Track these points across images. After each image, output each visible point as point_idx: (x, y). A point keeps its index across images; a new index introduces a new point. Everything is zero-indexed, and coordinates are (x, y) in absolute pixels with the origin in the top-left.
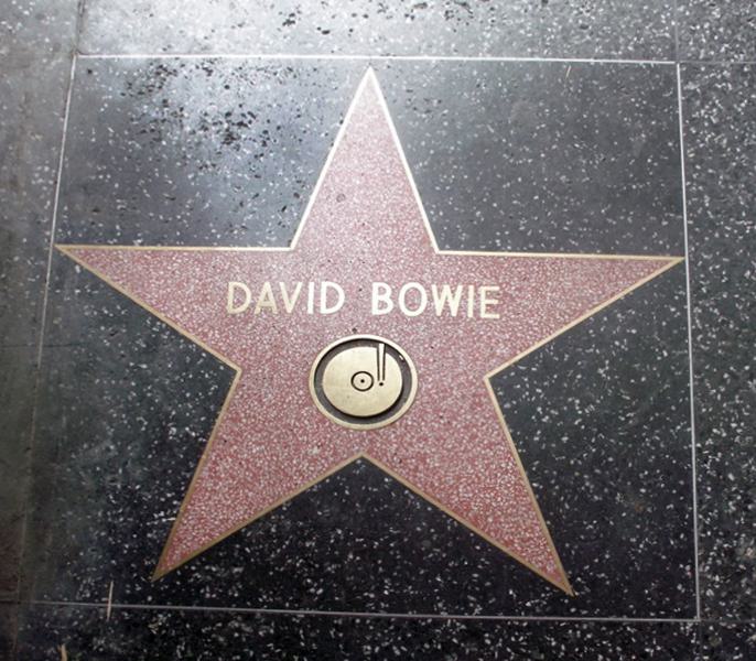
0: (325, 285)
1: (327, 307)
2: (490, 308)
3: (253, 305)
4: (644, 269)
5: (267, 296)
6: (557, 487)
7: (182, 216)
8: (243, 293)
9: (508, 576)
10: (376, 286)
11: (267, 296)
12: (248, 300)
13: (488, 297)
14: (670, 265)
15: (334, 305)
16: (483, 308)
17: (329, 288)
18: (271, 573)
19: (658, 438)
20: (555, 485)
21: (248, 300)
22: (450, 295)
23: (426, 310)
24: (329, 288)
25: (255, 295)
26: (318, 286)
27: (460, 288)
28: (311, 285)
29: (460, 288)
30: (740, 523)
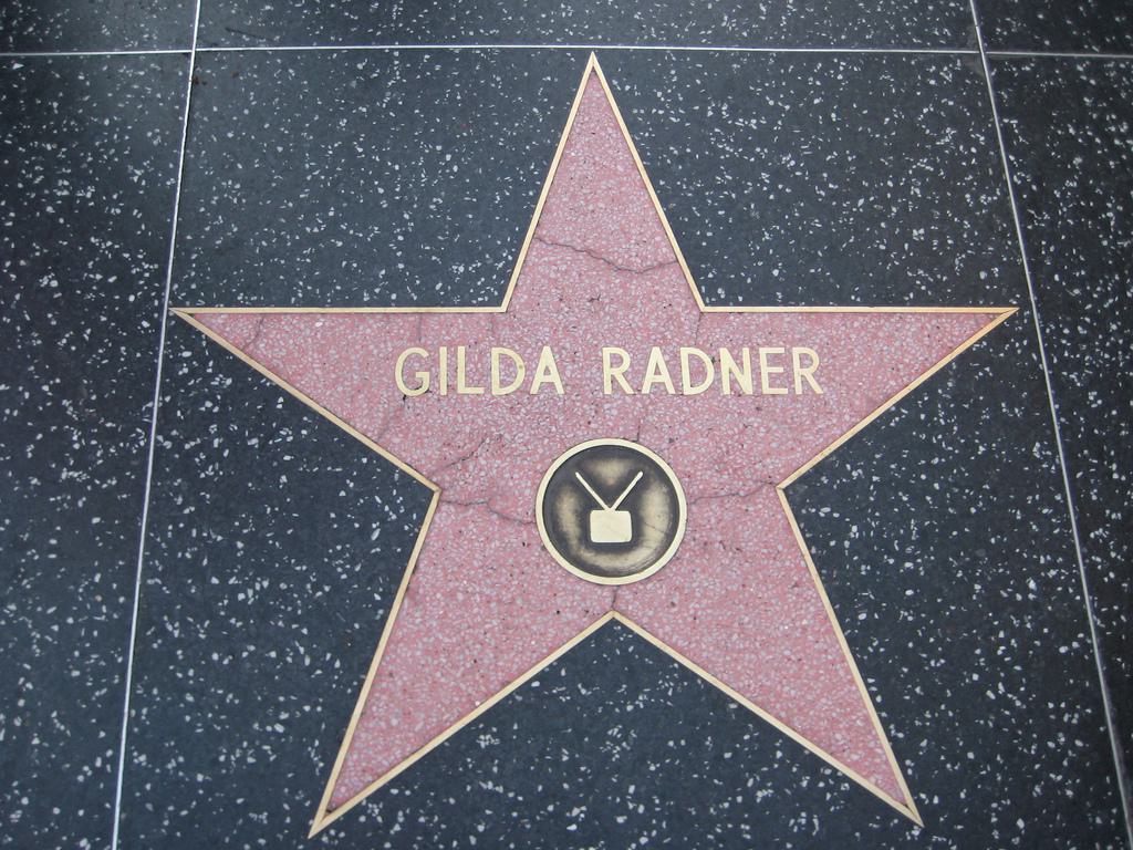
0: (685, 352)
2: (773, 379)
3: (528, 382)
4: (594, 89)
9: (970, 382)
10: (607, 352)
17: (692, 357)
18: (1099, 152)
19: (1000, 686)
21: (521, 374)
22: (736, 370)
23: (711, 388)
24: (692, 357)
25: (530, 371)
29: (746, 351)
30: (1045, 557)
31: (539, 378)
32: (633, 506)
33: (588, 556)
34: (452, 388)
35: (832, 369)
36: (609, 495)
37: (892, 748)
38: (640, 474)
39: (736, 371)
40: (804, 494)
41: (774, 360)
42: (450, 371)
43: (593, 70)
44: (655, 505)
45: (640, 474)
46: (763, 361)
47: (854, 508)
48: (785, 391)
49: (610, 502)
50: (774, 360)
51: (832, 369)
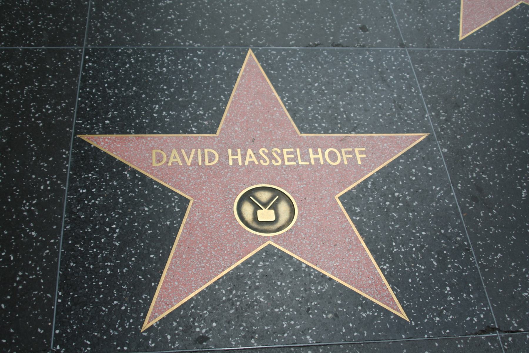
0: (206, 151)
1: (209, 162)
5: (175, 155)
6: (261, 270)
7: (447, 10)
8: (214, 156)
11: (175, 155)
12: (165, 160)
13: (288, 154)
14: (422, 139)
15: (213, 161)
16: (286, 160)
20: (116, 228)
21: (165, 160)
25: (168, 157)
26: (203, 150)
27: (193, 151)
28: (199, 151)
31: (172, 160)
32: (274, 207)
33: (259, 227)
34: (203, 161)
35: (359, 156)
36: (265, 205)
37: (164, 318)
38: (277, 197)
39: (320, 156)
40: (349, 200)
41: (288, 153)
42: (175, 158)
43: (462, 36)
44: (283, 207)
45: (277, 197)
46: (344, 154)
47: (373, 207)
48: (308, 163)
49: (266, 208)
50: (288, 153)
51: (359, 156)
